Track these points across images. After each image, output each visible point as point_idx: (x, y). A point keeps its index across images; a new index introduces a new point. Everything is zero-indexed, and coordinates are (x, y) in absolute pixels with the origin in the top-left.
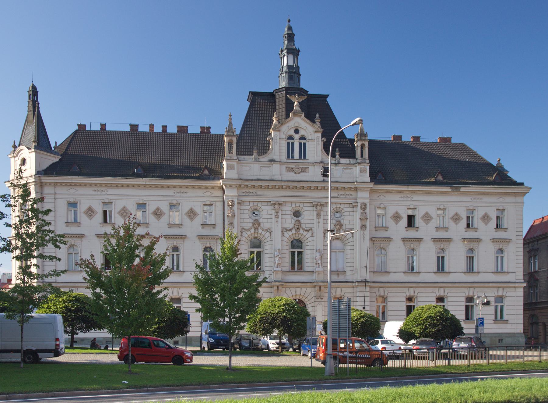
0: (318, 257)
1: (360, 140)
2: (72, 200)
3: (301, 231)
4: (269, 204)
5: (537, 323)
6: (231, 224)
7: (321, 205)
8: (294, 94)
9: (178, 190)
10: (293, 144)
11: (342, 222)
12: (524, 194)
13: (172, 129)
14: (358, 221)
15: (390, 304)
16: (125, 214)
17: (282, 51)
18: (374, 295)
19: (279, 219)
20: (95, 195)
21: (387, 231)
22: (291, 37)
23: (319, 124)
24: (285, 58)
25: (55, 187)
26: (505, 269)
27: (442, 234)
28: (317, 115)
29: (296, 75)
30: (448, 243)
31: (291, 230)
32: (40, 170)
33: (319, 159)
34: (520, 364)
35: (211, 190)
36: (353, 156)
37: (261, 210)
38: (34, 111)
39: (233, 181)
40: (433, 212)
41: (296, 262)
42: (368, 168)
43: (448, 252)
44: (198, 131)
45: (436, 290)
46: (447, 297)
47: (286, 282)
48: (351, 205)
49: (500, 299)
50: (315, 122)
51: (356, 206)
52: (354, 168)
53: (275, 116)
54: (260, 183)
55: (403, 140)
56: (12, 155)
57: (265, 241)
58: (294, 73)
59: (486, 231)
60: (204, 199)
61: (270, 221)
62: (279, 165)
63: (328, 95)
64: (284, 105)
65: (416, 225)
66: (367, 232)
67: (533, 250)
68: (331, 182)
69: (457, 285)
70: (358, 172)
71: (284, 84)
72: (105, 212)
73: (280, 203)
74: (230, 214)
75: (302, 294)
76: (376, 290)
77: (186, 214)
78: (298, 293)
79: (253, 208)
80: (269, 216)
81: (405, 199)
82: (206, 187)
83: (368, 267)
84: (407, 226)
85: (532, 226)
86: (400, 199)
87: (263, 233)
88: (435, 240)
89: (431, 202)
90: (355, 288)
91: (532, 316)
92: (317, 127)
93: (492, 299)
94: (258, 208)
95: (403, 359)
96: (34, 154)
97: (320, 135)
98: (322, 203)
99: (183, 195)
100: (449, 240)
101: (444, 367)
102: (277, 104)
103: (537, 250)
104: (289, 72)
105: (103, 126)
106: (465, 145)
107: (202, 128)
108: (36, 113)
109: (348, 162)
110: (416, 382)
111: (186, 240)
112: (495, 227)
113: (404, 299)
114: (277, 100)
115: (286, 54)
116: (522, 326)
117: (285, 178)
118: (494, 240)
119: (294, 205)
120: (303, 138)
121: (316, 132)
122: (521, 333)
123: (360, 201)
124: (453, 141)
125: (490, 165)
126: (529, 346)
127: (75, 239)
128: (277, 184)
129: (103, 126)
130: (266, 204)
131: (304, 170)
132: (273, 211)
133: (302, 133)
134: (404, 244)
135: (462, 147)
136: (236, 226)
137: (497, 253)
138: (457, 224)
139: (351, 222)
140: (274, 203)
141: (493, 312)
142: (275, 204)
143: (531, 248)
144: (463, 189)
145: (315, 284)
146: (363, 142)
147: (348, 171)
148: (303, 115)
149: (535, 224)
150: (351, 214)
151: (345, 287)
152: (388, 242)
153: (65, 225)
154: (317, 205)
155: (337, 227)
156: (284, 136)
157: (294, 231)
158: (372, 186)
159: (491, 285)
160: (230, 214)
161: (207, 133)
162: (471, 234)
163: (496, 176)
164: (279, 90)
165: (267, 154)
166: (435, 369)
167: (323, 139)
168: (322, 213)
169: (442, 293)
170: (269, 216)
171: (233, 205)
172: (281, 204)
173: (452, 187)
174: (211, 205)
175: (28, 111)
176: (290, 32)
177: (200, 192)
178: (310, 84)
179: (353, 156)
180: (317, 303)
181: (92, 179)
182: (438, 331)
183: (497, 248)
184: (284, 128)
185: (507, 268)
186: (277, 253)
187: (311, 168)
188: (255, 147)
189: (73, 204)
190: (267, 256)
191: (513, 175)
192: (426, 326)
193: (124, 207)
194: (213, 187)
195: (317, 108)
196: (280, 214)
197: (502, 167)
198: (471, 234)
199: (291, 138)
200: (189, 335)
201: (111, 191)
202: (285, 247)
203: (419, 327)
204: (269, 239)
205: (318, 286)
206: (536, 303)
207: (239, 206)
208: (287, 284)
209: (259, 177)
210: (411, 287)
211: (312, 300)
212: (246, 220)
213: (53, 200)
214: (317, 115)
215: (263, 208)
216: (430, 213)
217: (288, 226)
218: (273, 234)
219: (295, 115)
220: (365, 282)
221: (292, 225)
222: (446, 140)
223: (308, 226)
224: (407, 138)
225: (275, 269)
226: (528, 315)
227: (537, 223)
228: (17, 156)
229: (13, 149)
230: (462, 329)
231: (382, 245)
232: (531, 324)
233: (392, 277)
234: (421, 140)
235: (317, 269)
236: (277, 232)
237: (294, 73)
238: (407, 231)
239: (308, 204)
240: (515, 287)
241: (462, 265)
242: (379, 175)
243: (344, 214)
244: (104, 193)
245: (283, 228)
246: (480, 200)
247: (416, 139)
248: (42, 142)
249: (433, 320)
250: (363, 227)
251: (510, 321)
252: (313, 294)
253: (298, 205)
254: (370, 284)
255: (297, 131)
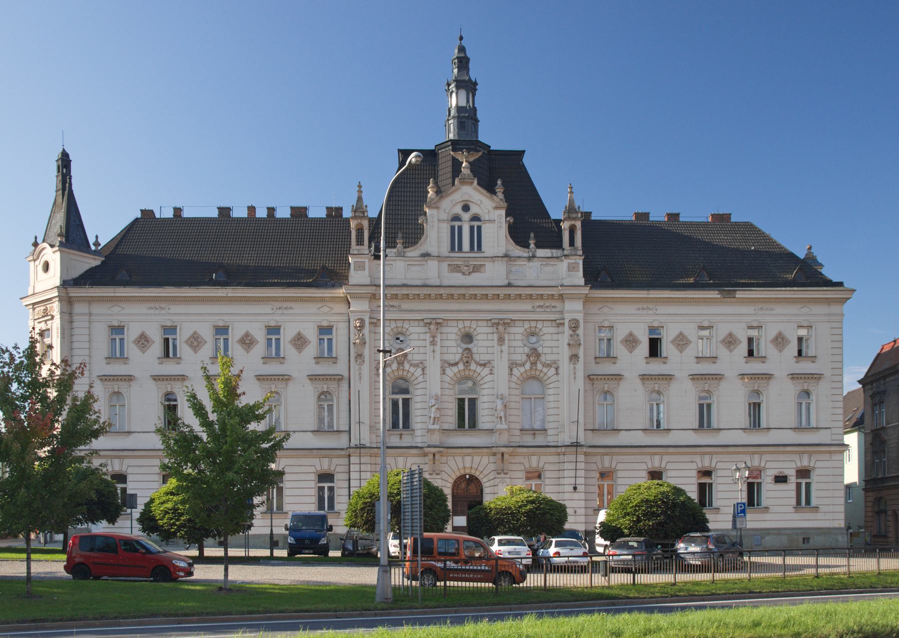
0: (500, 406)
1: (569, 218)
2: (116, 324)
3: (473, 366)
4: (421, 323)
5: (885, 512)
6: (360, 356)
7: (504, 324)
8: (461, 150)
9: (278, 305)
10: (460, 228)
11: (540, 350)
12: (844, 300)
13: (283, 213)
14: (566, 347)
15: (620, 481)
16: (195, 344)
17: (449, 85)
18: (594, 467)
19: (438, 348)
20: (151, 315)
21: (615, 363)
22: (463, 63)
23: (501, 195)
24: (454, 95)
25: (90, 304)
26: (813, 424)
27: (706, 368)
28: (499, 182)
29: (470, 122)
30: (716, 382)
31: (456, 364)
32: (66, 278)
33: (501, 251)
34: (777, 581)
35: (330, 304)
36: (558, 245)
37: (408, 333)
38: (64, 190)
39: (363, 288)
40: (691, 331)
41: (467, 415)
42: (581, 263)
43: (722, 398)
44: (323, 214)
45: (697, 458)
46: (715, 469)
47: (448, 448)
48: (554, 324)
49: (804, 473)
50: (494, 193)
51: (563, 324)
52: (559, 264)
53: (431, 185)
54: (405, 291)
55: (651, 219)
56: (31, 258)
57: (415, 382)
58: (467, 118)
59: (780, 362)
60: (319, 318)
61: (422, 350)
62: (436, 262)
63: (524, 151)
64: (450, 169)
65: (664, 354)
66: (580, 366)
67: (878, 393)
68: (386, 286)
69: (731, 449)
70: (565, 269)
71: (451, 136)
72: (166, 341)
73: (439, 321)
74: (358, 341)
75: (475, 466)
76: (598, 459)
77: (291, 342)
78: (468, 465)
79: (395, 330)
80: (422, 343)
81: (645, 312)
82: (322, 299)
83: (581, 420)
84: (647, 354)
85: (879, 355)
86: (637, 312)
87: (412, 370)
88: (695, 377)
89: (694, 319)
90: (561, 457)
91: (878, 500)
92: (498, 200)
93: (791, 473)
94: (404, 330)
95: (542, 572)
96: (58, 254)
97: (503, 212)
98: (507, 321)
99: (285, 312)
100: (718, 377)
101: (622, 587)
102: (440, 167)
103: (884, 392)
104: (459, 117)
105: (178, 211)
106: (752, 225)
107: (329, 209)
108: (66, 192)
109: (549, 255)
110: (581, 612)
111: (290, 383)
112: (796, 354)
113: (694, 473)
114: (440, 161)
115: (454, 89)
116: (842, 516)
117: (446, 283)
118: (794, 377)
119: (461, 325)
120: (476, 218)
121: (496, 208)
122: (840, 529)
123: (568, 317)
124: (734, 219)
125: (791, 256)
126: (853, 551)
127: (120, 383)
128: (433, 292)
129: (178, 211)
130: (416, 323)
131: (477, 269)
132: (428, 335)
133: (474, 209)
134: (643, 384)
135: (748, 228)
136: (367, 359)
137: (799, 396)
138: (731, 351)
139: (555, 350)
140: (496, 321)
141: (793, 494)
142: (430, 324)
143: (875, 390)
144: (740, 294)
145: (494, 450)
146: (573, 222)
147: (549, 269)
148: (476, 182)
149: (884, 351)
150: (555, 337)
151: (546, 454)
152: (616, 382)
153: (105, 361)
154: (498, 324)
155: (532, 359)
156: (444, 216)
157: (461, 366)
158: (587, 292)
159: (788, 449)
160: (358, 341)
161: (336, 216)
162: (755, 367)
163: (806, 274)
164: (443, 146)
165: (418, 245)
166: (607, 591)
167: (508, 219)
168: (506, 336)
169: (706, 464)
170: (422, 343)
171: (362, 326)
172: (440, 323)
173: (721, 292)
174: (710, 328)
175: (57, 191)
176: (462, 55)
177: (312, 308)
178: (494, 135)
179: (558, 245)
180: (497, 480)
181: (144, 290)
182: (659, 524)
183: (800, 388)
184: (446, 203)
185: (817, 421)
186: (433, 402)
187: (489, 265)
188: (400, 235)
189: (117, 330)
190: (419, 406)
191: (828, 272)
192: (638, 516)
193: (195, 333)
194: (333, 299)
195: (502, 171)
196: (438, 339)
197: (814, 259)
198: (755, 367)
199: (456, 218)
200: (253, 531)
201: (176, 309)
202: (447, 392)
203: (628, 518)
204: (421, 379)
205: (501, 456)
206: (884, 480)
207: (373, 328)
208: (450, 451)
209: (405, 282)
210: (656, 454)
211: (491, 476)
212: (518, 350)
213: (86, 324)
214: (499, 182)
215: (412, 330)
216: (686, 333)
217: (453, 358)
218: (427, 371)
219: (463, 182)
220: (577, 446)
221: (458, 357)
222: (722, 219)
223: (484, 358)
224: (658, 215)
225: (431, 427)
226: (871, 499)
227: (886, 349)
228: (38, 258)
229: (33, 248)
230: (706, 521)
231: (606, 386)
232: (877, 513)
233: (624, 438)
234: (681, 219)
235: (499, 426)
236: (434, 368)
237: (467, 118)
238: (647, 363)
239: (485, 324)
240: (830, 452)
241: (742, 417)
242: (598, 275)
243: (543, 338)
244: (163, 312)
245: (444, 362)
246: (770, 312)
247: (674, 217)
248: (73, 235)
249: (651, 507)
250: (574, 357)
251: (822, 508)
252: (492, 467)
253: (467, 324)
254: (585, 449)
255: (466, 208)
